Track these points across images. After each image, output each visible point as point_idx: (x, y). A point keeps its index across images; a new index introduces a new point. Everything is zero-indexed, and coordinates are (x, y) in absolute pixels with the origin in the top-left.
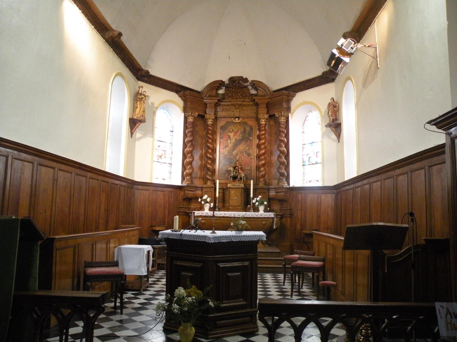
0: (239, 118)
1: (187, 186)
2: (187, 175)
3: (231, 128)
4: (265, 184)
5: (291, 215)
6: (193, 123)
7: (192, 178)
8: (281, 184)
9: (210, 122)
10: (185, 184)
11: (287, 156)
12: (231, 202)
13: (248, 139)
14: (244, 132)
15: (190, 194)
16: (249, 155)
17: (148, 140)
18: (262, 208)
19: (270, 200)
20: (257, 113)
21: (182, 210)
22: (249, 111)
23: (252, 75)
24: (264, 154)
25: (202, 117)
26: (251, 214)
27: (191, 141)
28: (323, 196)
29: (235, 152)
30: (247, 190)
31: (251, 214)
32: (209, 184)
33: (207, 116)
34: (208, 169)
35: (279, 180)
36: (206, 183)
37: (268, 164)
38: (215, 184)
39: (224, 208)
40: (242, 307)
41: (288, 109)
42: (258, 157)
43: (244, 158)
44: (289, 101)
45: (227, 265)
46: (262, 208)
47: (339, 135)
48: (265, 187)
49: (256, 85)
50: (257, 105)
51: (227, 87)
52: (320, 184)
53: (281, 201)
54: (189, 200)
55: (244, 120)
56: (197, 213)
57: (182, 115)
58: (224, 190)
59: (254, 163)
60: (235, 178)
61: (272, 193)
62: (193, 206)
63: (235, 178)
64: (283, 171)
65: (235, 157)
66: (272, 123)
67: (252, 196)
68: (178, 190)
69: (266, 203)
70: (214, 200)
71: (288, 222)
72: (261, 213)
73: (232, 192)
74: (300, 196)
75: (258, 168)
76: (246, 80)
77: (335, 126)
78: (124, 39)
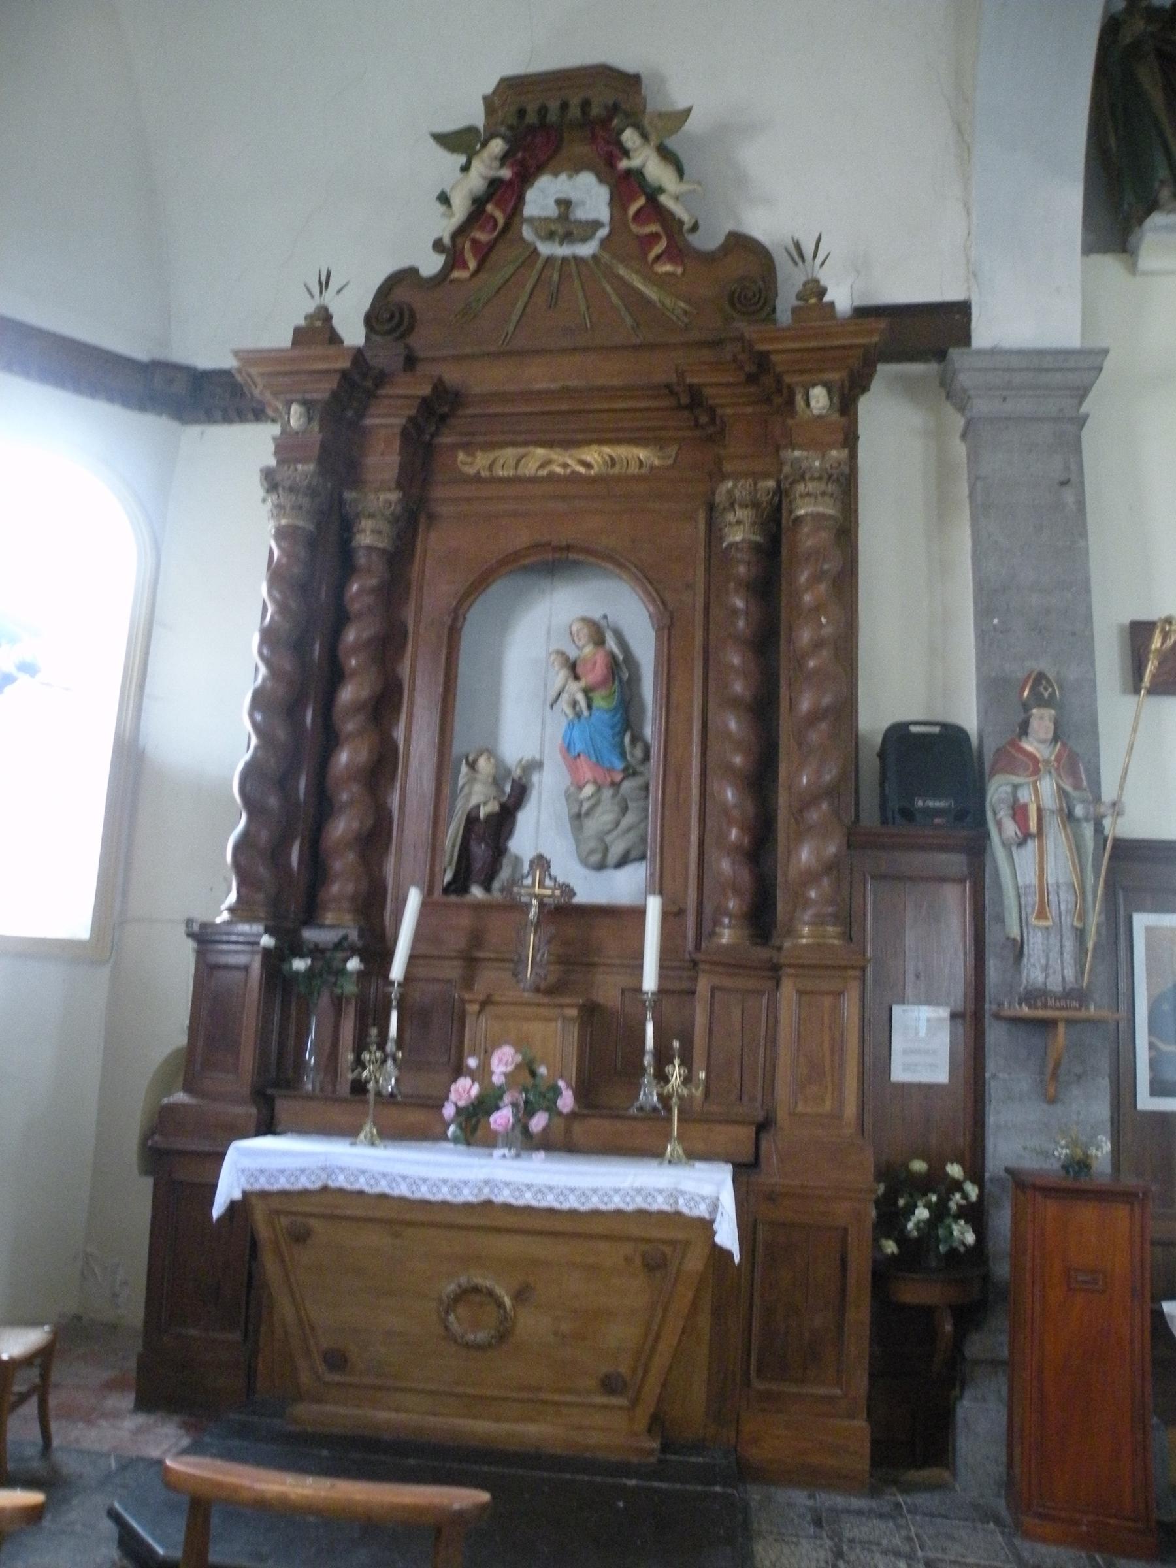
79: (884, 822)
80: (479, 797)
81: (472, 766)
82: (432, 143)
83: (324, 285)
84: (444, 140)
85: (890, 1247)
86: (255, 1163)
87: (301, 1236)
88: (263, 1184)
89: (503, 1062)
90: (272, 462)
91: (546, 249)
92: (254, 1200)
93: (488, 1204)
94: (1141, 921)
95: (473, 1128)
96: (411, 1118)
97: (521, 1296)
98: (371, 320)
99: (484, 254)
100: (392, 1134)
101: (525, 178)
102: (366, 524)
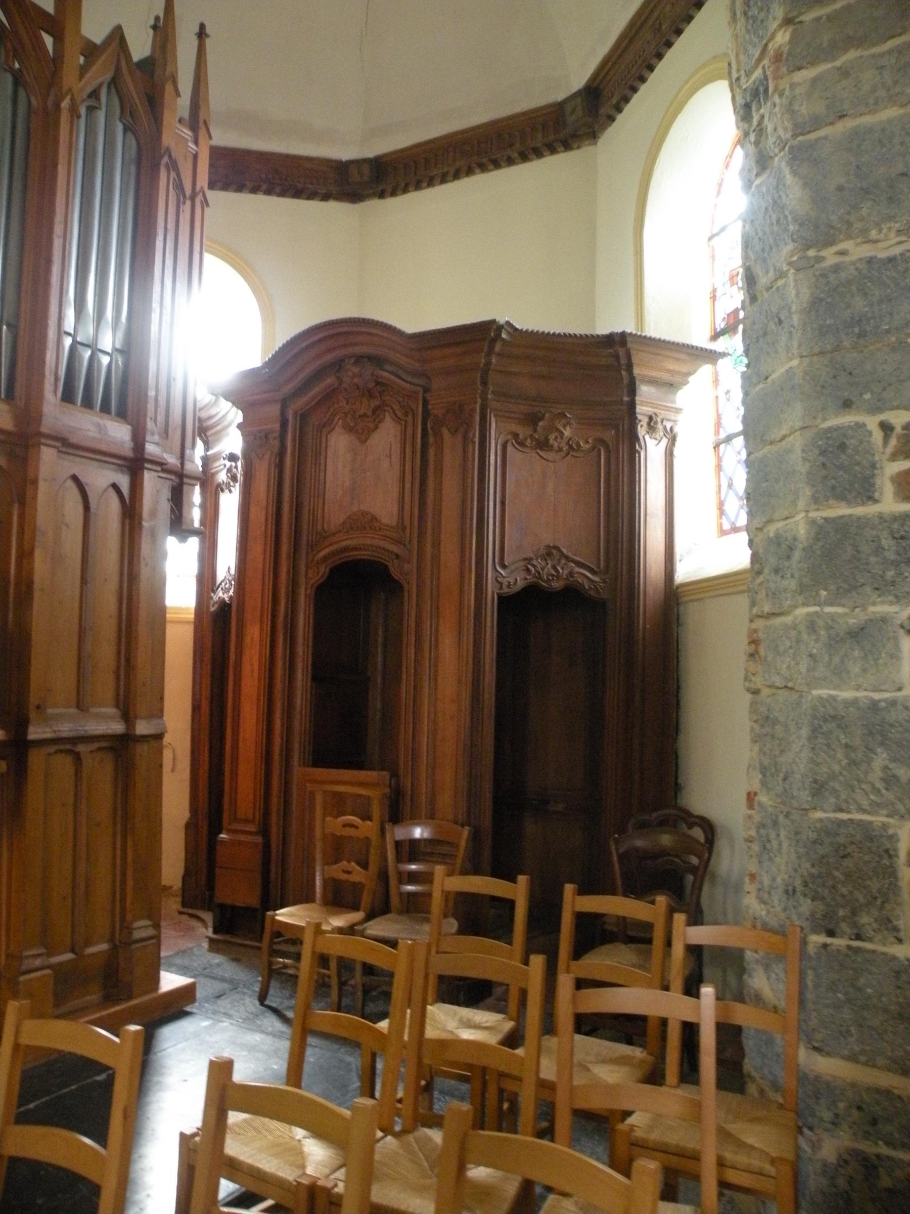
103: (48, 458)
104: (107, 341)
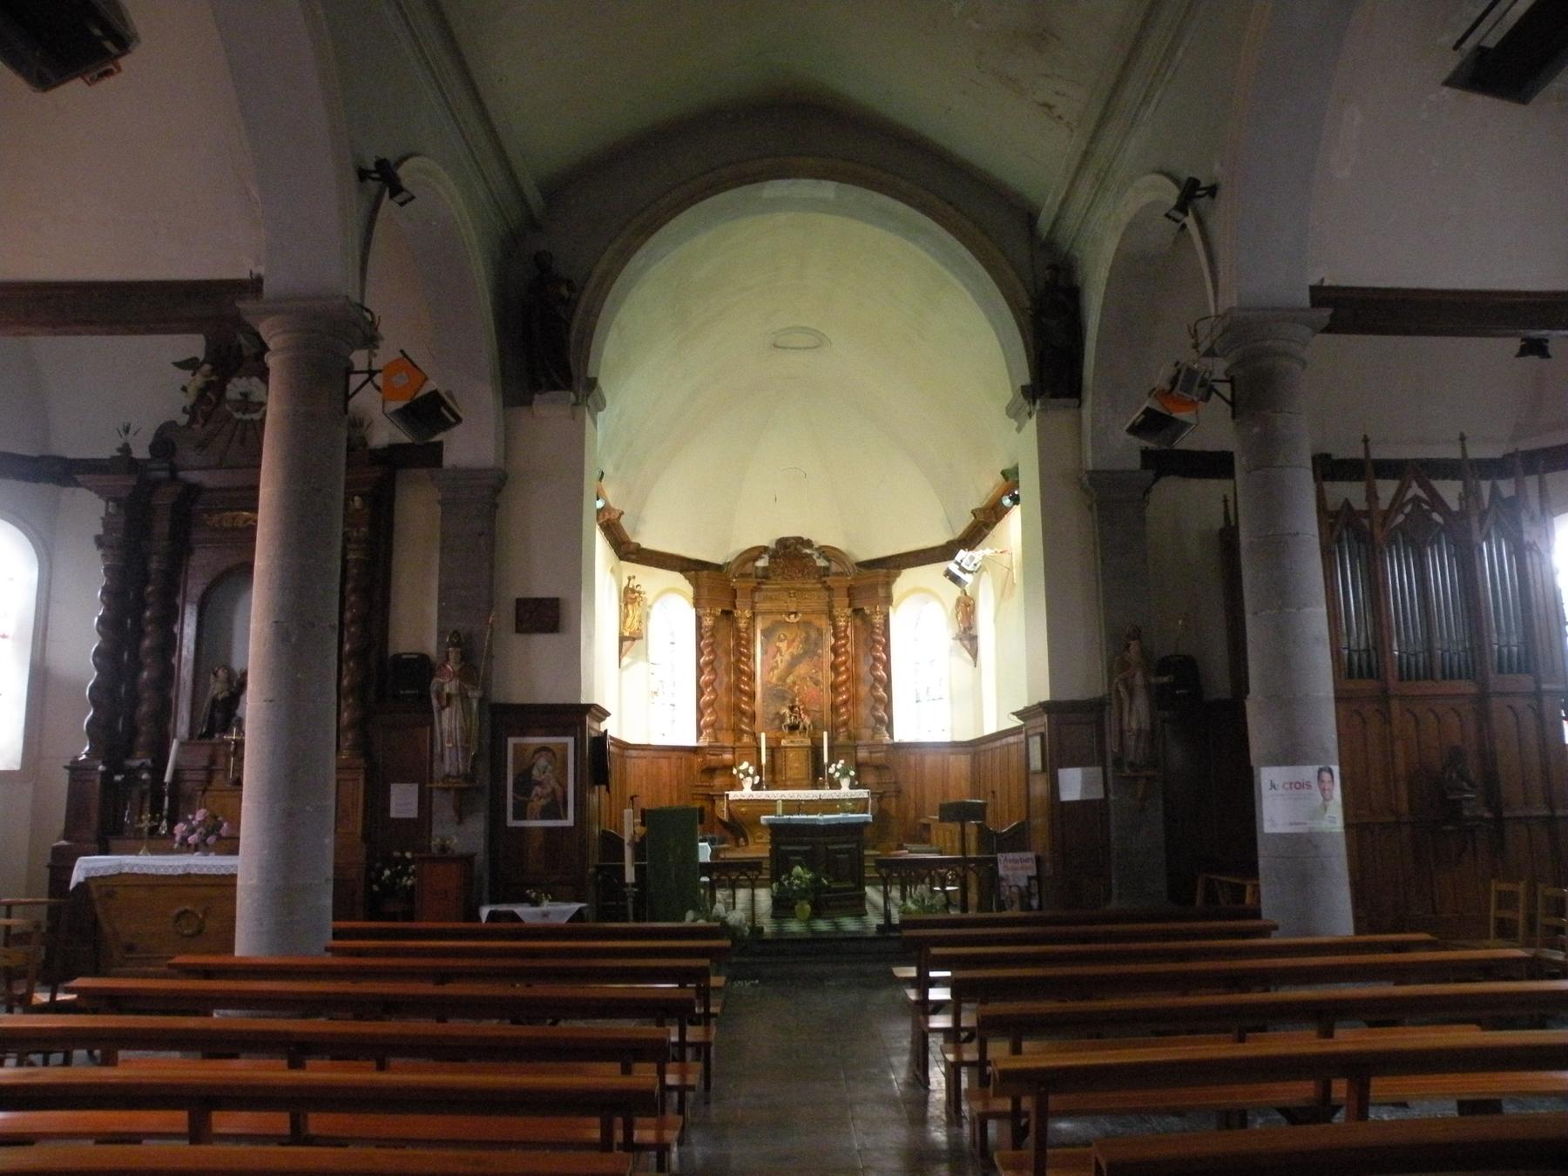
0: (796, 613)
1: (710, 747)
2: (707, 726)
3: (781, 633)
4: (849, 737)
5: (899, 792)
6: (713, 628)
7: (715, 731)
8: (877, 737)
9: (742, 624)
10: (704, 742)
11: (888, 687)
12: (790, 773)
13: (815, 653)
14: (807, 639)
15: (712, 760)
16: (817, 683)
17: (641, 666)
18: (845, 783)
19: (859, 766)
20: (831, 607)
21: (701, 790)
22: (816, 601)
23: (823, 536)
24: (845, 682)
25: (727, 614)
26: (827, 793)
27: (711, 663)
28: (952, 758)
29: (789, 680)
30: (816, 751)
31: (827, 793)
32: (746, 739)
33: (737, 613)
34: (743, 713)
35: (875, 731)
36: (739, 739)
37: (854, 700)
38: (757, 739)
39: (773, 784)
40: (851, 889)
41: (888, 600)
42: (835, 688)
43: (809, 689)
44: (888, 585)
45: (580, 1024)
46: (845, 783)
47: (974, 653)
48: (851, 743)
49: (828, 552)
50: (829, 589)
51: (774, 556)
52: (946, 737)
53: (879, 768)
54: (710, 771)
55: (807, 618)
56: (733, 795)
57: (692, 613)
58: (772, 751)
59: (827, 697)
60: (793, 728)
61: (862, 754)
62: (719, 781)
63: (793, 728)
64: (881, 713)
65: (791, 688)
66: (859, 622)
67: (826, 760)
68: (692, 756)
69: (852, 773)
70: (759, 771)
71: (892, 806)
72: (845, 791)
73: (791, 755)
74: (912, 759)
75: (835, 708)
76: (809, 544)
77: (968, 637)
78: (624, 521)
79: (1328, 468)
80: (217, 688)
81: (215, 674)
82: (176, 369)
83: (127, 430)
84: (182, 365)
85: (375, 888)
86: (85, 867)
87: (111, 895)
88: (93, 874)
89: (200, 815)
90: (100, 531)
91: (238, 416)
92: (93, 886)
93: (188, 875)
94: (511, 741)
95: (186, 848)
96: (158, 842)
97: (205, 913)
98: (152, 448)
99: (207, 417)
100: (154, 851)
101: (225, 380)
102: (155, 558)
103: (1495, 702)
104: (1514, 640)
